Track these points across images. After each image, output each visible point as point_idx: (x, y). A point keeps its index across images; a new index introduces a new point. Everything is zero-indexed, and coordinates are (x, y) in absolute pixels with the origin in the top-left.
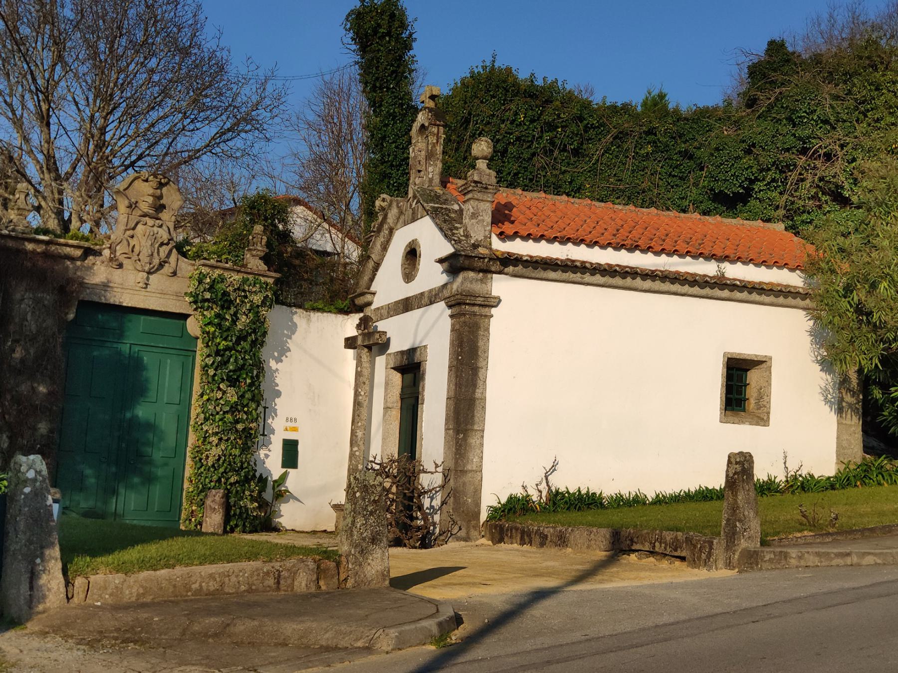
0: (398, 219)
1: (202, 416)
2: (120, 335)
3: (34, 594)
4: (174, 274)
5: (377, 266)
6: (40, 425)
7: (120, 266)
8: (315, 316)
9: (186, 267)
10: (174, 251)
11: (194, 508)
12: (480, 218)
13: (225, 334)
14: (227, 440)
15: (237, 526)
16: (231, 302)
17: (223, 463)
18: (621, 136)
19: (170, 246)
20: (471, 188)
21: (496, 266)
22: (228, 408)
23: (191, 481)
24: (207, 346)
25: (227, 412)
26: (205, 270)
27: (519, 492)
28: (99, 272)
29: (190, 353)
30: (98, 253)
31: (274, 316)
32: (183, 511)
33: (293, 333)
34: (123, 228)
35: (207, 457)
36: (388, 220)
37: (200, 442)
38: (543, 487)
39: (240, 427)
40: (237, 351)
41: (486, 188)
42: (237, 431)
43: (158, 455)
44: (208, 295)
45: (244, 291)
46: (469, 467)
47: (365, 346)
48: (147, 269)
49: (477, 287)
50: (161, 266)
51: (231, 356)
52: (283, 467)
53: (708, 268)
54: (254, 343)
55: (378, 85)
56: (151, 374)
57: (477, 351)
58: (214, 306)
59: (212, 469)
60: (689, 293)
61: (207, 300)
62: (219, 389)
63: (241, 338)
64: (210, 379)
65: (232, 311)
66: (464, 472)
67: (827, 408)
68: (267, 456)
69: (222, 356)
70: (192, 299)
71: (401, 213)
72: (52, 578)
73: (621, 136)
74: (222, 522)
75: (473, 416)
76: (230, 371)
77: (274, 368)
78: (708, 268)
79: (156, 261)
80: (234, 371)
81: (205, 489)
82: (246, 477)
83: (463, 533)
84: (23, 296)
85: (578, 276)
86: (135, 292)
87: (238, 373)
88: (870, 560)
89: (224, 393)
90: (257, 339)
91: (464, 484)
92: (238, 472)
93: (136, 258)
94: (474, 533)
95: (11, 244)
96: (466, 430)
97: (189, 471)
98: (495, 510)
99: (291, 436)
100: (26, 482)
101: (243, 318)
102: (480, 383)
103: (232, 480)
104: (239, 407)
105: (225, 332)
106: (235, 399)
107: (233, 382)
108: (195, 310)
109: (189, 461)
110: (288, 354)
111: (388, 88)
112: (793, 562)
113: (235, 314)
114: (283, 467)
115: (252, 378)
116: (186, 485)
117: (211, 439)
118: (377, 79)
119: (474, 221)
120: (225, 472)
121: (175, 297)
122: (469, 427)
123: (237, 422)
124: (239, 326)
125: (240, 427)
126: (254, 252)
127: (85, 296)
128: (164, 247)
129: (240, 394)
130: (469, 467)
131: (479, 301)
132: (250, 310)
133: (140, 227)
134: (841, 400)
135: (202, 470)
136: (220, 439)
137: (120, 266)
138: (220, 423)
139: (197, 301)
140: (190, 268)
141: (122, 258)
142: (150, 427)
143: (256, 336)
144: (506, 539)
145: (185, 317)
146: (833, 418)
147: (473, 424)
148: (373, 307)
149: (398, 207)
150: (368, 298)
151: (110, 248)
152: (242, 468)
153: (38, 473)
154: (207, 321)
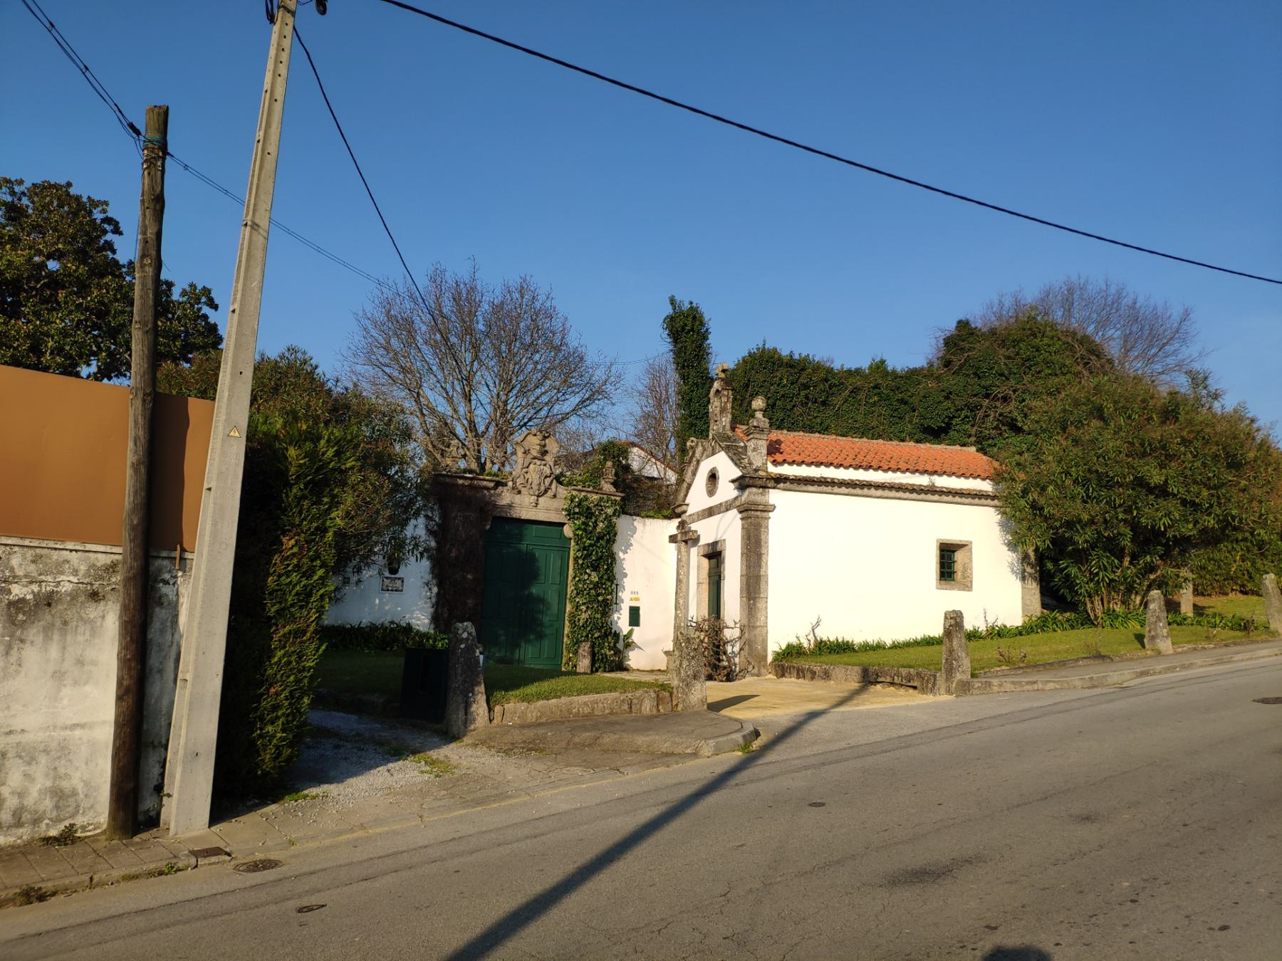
2: (520, 538)
3: (468, 719)
4: (555, 496)
7: (519, 492)
8: (648, 521)
9: (563, 491)
18: (855, 391)
26: (574, 493)
27: (794, 641)
28: (506, 497)
31: (622, 523)
38: (811, 637)
39: (600, 598)
43: (546, 620)
49: (759, 499)
50: (546, 491)
53: (923, 480)
56: (541, 564)
63: (600, 538)
66: (755, 627)
67: (1014, 577)
72: (479, 707)
73: (855, 391)
78: (923, 480)
79: (543, 488)
81: (577, 643)
83: (755, 671)
85: (829, 489)
88: (1051, 686)
94: (763, 671)
95: (448, 480)
97: (567, 630)
98: (778, 654)
99: (635, 604)
100: (462, 641)
107: (595, 568)
112: (996, 689)
123: (598, 595)
127: (496, 513)
131: (761, 507)
134: (1024, 571)
137: (519, 492)
139: (571, 514)
142: (541, 600)
143: (610, 536)
145: (563, 525)
146: (1018, 584)
150: (684, 508)
153: (470, 634)
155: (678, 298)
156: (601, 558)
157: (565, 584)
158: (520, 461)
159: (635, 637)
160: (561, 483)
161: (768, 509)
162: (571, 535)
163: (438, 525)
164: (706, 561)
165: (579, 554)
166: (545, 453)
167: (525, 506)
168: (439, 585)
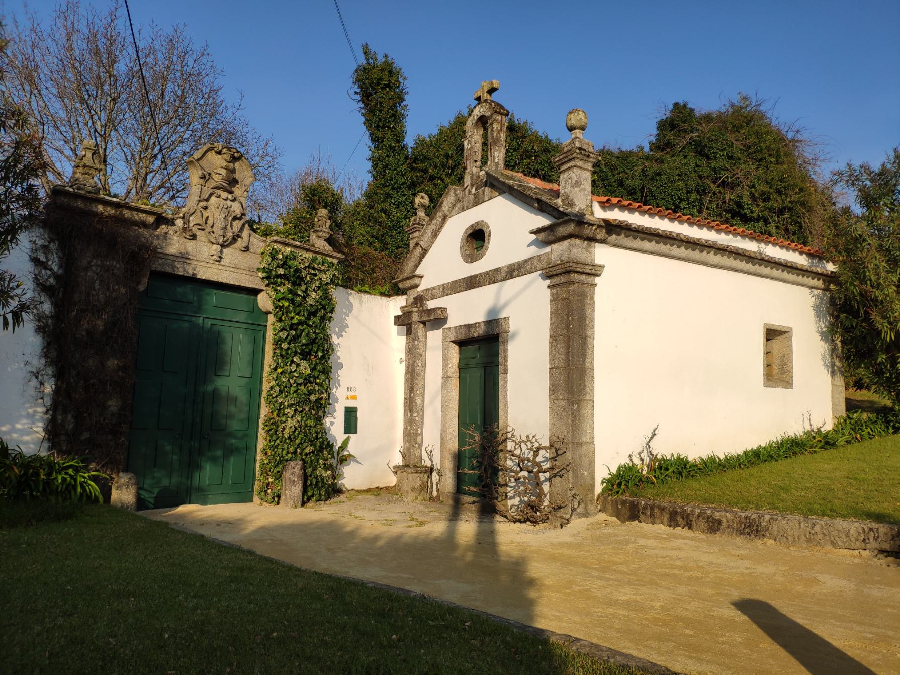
0: (454, 206)
1: (277, 389)
4: (247, 249)
5: (425, 252)
6: (110, 403)
7: (194, 237)
8: (365, 297)
9: (258, 243)
10: (247, 226)
11: (270, 480)
12: (582, 186)
13: (298, 309)
14: (301, 412)
15: (313, 496)
16: (302, 279)
17: (299, 434)
19: (243, 221)
20: (575, 155)
21: (601, 234)
22: (301, 381)
23: (266, 453)
24: (280, 320)
25: (300, 384)
26: (277, 246)
27: (625, 461)
28: (175, 245)
29: (260, 328)
30: (171, 222)
31: (337, 294)
32: (257, 483)
33: (351, 311)
34: (197, 198)
35: (284, 429)
36: (443, 208)
37: (275, 414)
38: (645, 455)
39: (313, 398)
40: (308, 325)
41: (588, 156)
42: (310, 401)
44: (281, 271)
45: (314, 268)
46: (584, 439)
47: (421, 322)
48: (221, 241)
50: (234, 239)
51: (303, 331)
52: (345, 433)
54: (323, 318)
55: (381, 124)
57: (585, 319)
58: (286, 282)
59: (288, 441)
60: (744, 269)
61: (280, 276)
62: (293, 362)
64: (284, 353)
65: (303, 287)
66: (580, 444)
67: (825, 371)
68: (332, 423)
69: (296, 330)
70: (265, 274)
71: (458, 200)
74: (301, 494)
75: (584, 386)
76: (303, 345)
77: (336, 342)
79: (229, 235)
80: (306, 345)
81: (281, 462)
82: (321, 447)
84: (89, 262)
86: (209, 265)
87: (310, 347)
89: (298, 365)
90: (324, 315)
91: (581, 456)
92: (312, 443)
93: (209, 229)
94: (591, 508)
95: (80, 204)
96: (580, 401)
97: (261, 443)
98: (609, 481)
99: (351, 404)
101: (314, 295)
102: (589, 352)
103: (307, 450)
104: (312, 379)
105: (297, 306)
106: (308, 371)
107: (305, 355)
108: (267, 285)
109: (261, 432)
110: (347, 330)
111: (389, 127)
113: (305, 292)
114: (345, 433)
115: (323, 351)
116: (259, 456)
117: (286, 411)
118: (380, 120)
119: (577, 189)
120: (301, 443)
121: (248, 272)
122: (582, 397)
123: (310, 393)
124: (310, 301)
125: (313, 398)
126: (320, 234)
127: (157, 266)
128: (237, 222)
129: (312, 366)
130: (584, 439)
131: (587, 269)
132: (319, 288)
133: (213, 199)
135: (278, 441)
136: (296, 411)
137: (194, 237)
138: (295, 395)
139: (271, 278)
140: (262, 244)
141: (195, 230)
143: (325, 310)
144: (642, 517)
145: (255, 292)
146: (829, 378)
147: (585, 394)
148: (420, 289)
149: (455, 194)
150: (417, 280)
151: (183, 218)
152: (317, 438)
154: (280, 296)
155: (372, 48)
156: (313, 342)
157: (251, 373)
158: (195, 190)
159: (351, 449)
160: (255, 231)
161: (595, 271)
162: (270, 308)
163: (57, 277)
164: (456, 348)
165: (283, 335)
166: (234, 182)
167: (206, 260)
168: (59, 376)
